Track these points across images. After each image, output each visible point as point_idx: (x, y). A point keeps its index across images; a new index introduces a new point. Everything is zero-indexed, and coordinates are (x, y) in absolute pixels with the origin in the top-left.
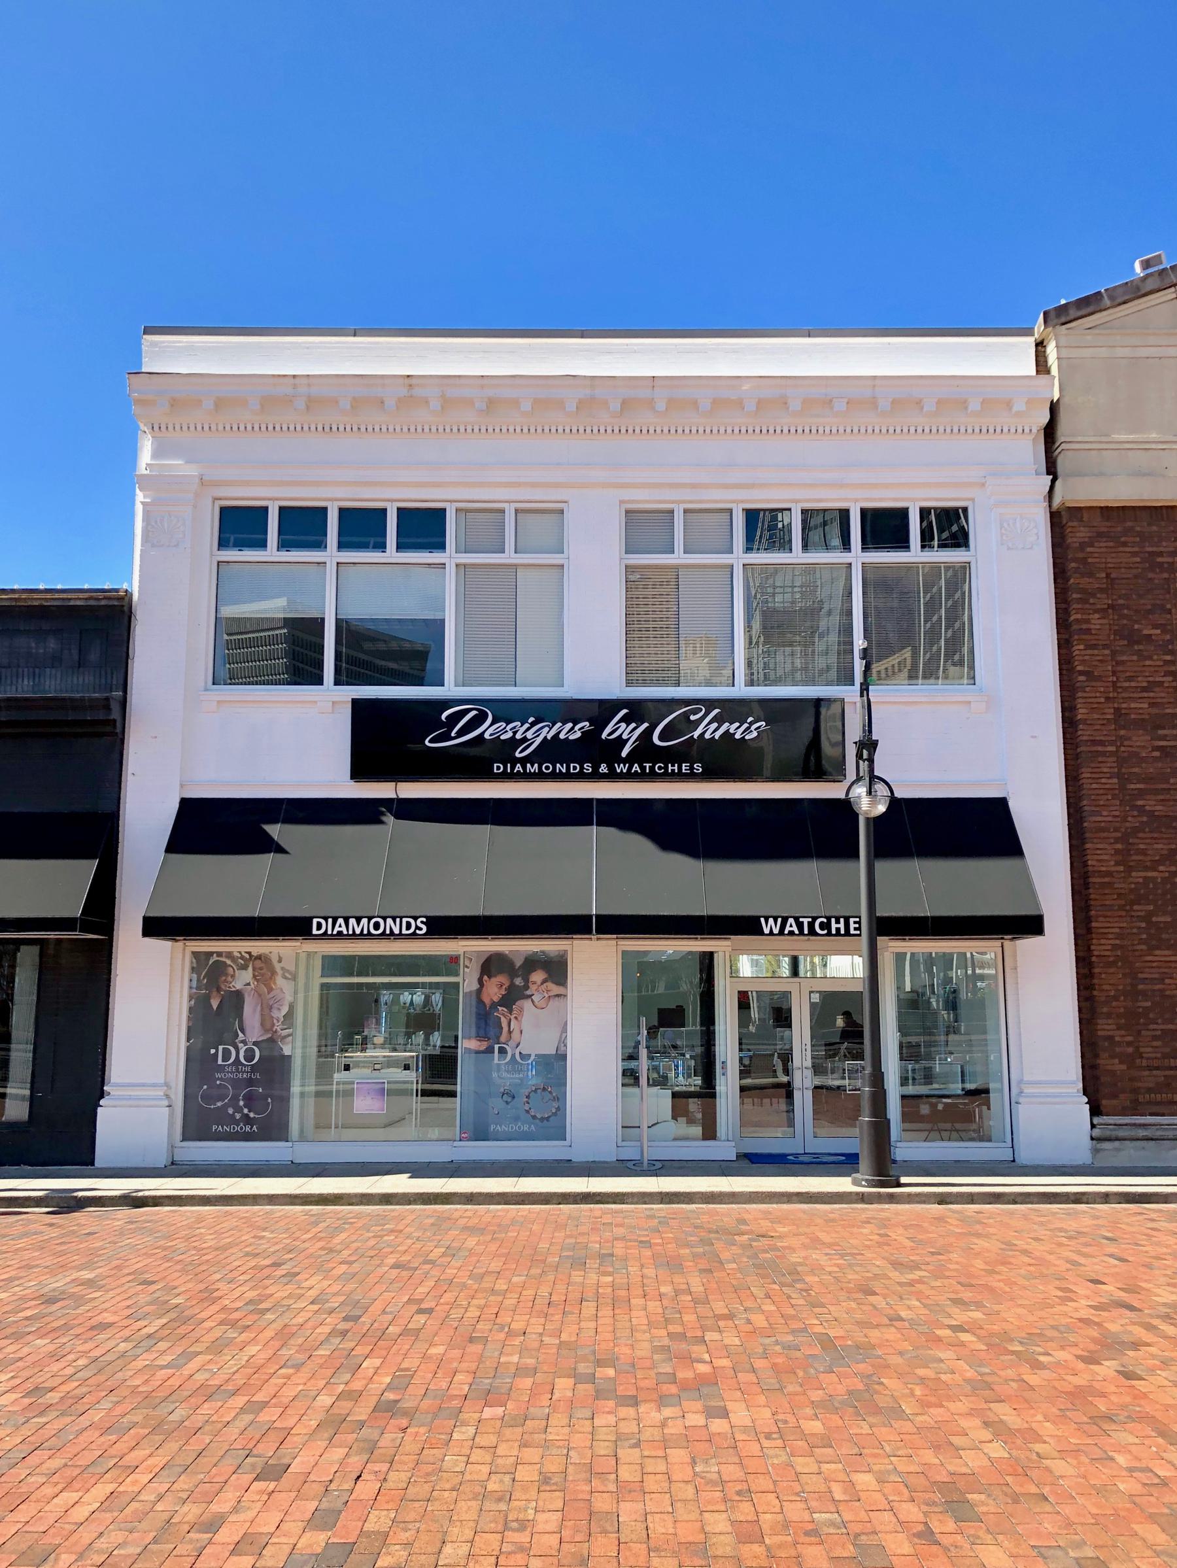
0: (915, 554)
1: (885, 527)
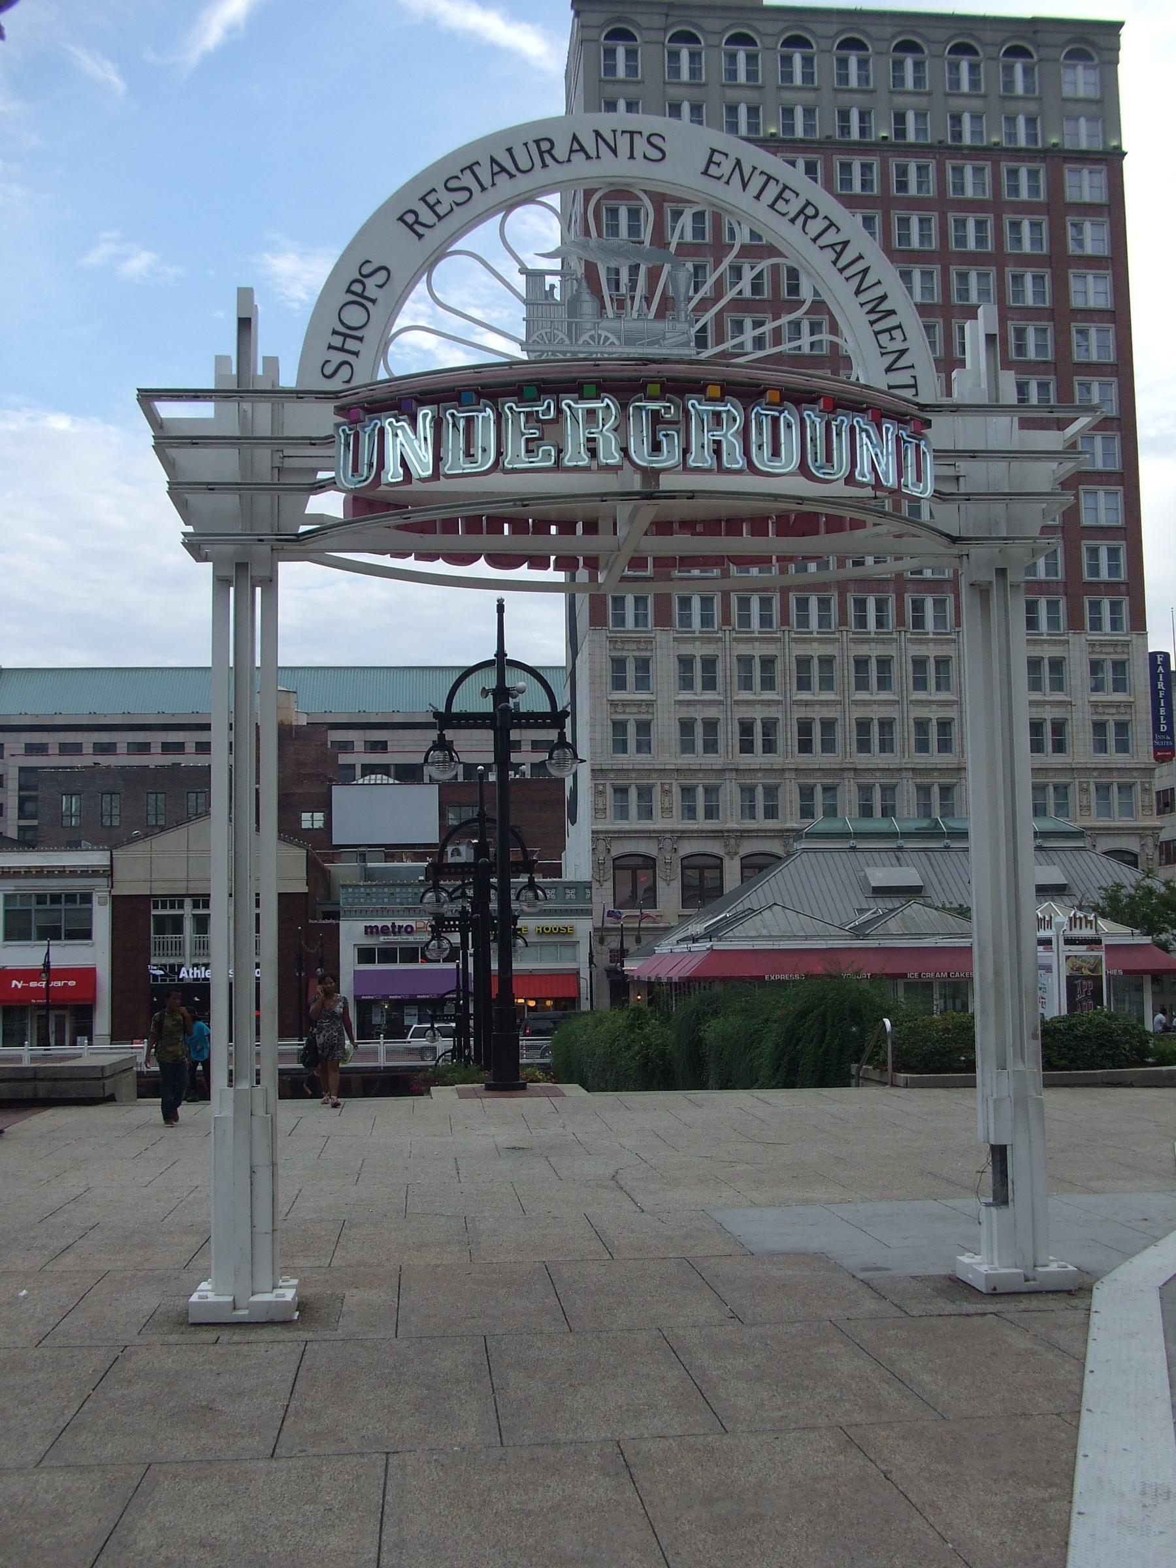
1: (71, 898)
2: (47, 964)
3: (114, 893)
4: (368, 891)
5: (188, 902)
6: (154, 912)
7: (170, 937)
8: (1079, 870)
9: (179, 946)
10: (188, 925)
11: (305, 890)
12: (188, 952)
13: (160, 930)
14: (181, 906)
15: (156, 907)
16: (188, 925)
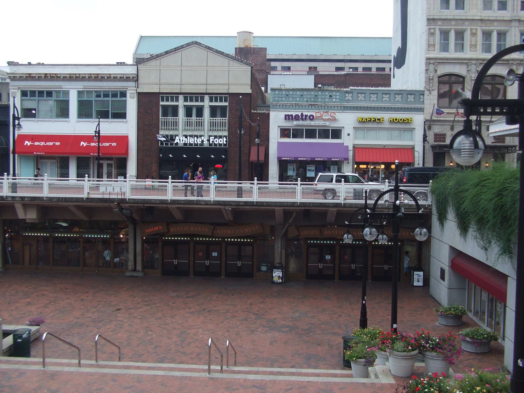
0: (118, 99)
1: (115, 95)
3: (140, 90)
6: (162, 103)
7: (170, 119)
9: (176, 124)
10: (181, 112)
11: (249, 91)
13: (165, 114)
14: (202, 100)
15: (163, 100)
16: (181, 112)
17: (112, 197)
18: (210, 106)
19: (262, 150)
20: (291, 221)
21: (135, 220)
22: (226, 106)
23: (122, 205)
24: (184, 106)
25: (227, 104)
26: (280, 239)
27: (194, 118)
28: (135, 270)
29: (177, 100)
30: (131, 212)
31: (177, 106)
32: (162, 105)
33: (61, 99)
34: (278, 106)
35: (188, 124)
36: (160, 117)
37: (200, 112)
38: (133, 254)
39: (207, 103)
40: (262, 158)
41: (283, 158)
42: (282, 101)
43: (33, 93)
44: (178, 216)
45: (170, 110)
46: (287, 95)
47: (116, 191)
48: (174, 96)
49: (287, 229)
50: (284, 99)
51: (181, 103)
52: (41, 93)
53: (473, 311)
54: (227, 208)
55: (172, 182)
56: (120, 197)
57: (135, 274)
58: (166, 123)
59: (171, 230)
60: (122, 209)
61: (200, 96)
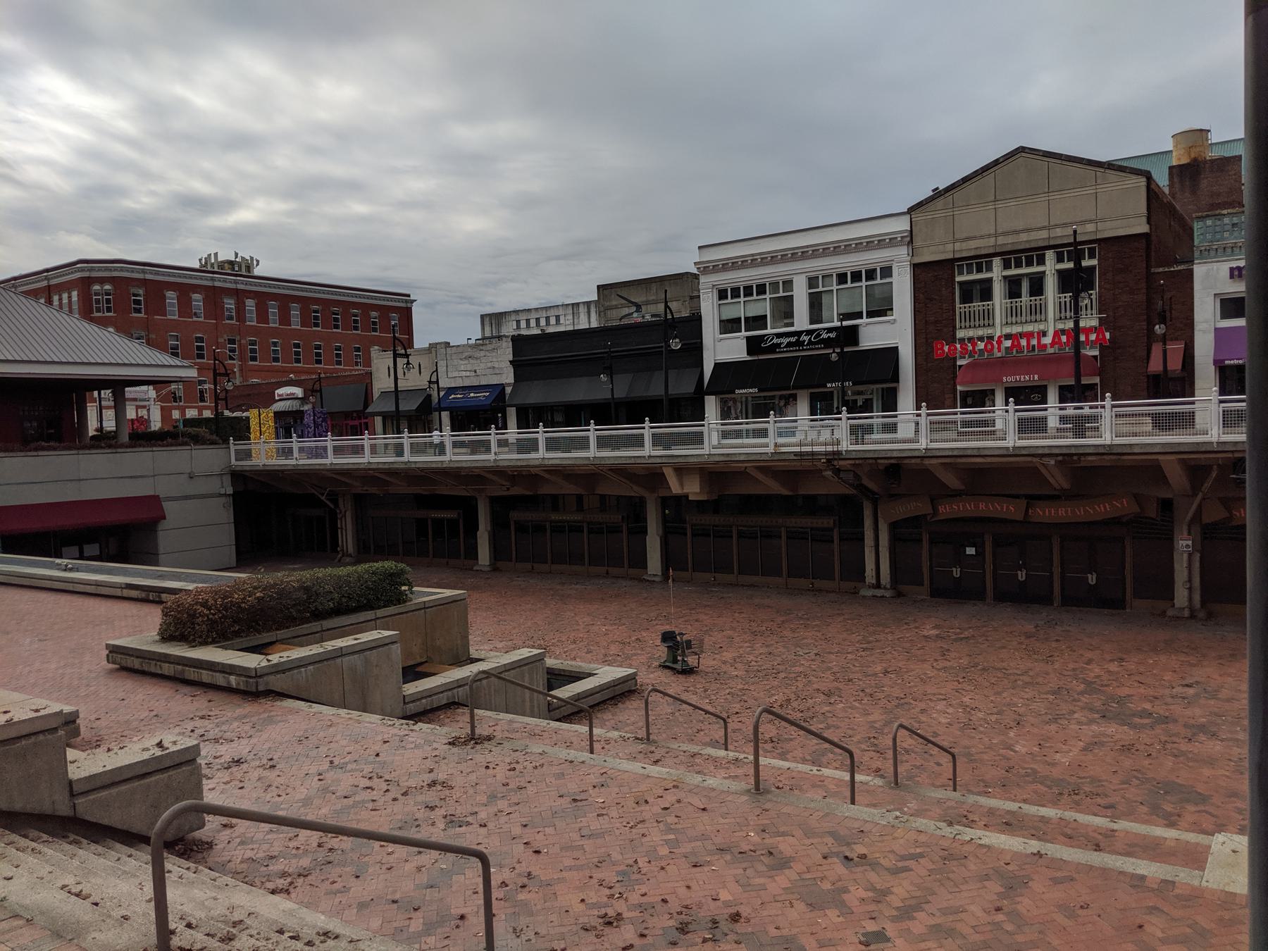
1: (871, 274)
2: (1165, 344)
3: (917, 260)
4: (1235, 220)
5: (997, 262)
6: (958, 279)
7: (977, 305)
8: (19, 343)
9: (989, 314)
10: (998, 290)
11: (1143, 228)
12: (998, 321)
13: (967, 298)
14: (1041, 261)
15: (961, 273)
16: (998, 290)
17: (816, 449)
18: (1059, 272)
19: (1176, 347)
20: (1207, 485)
21: (874, 493)
22: (1093, 268)
23: (835, 463)
24: (1005, 277)
25: (1094, 262)
26: (1185, 528)
27: (1025, 298)
28: (878, 586)
29: (989, 269)
30: (856, 476)
31: (990, 280)
32: (960, 283)
33: (781, 294)
34: (1212, 253)
35: (1013, 312)
36: (958, 305)
37: (1037, 286)
38: (877, 559)
39: (1051, 267)
40: (1175, 364)
41: (1227, 362)
42: (1223, 239)
43: (735, 292)
44: (952, 481)
45: (976, 291)
46: (1234, 225)
47: (822, 439)
48: (981, 261)
49: (1200, 506)
50: (1226, 235)
51: (997, 272)
52: (748, 291)
53: (926, 582)
54: (1045, 460)
55: (928, 415)
56: (830, 448)
57: (879, 593)
58: (968, 317)
59: (941, 509)
60: (837, 471)
61: (1035, 254)
